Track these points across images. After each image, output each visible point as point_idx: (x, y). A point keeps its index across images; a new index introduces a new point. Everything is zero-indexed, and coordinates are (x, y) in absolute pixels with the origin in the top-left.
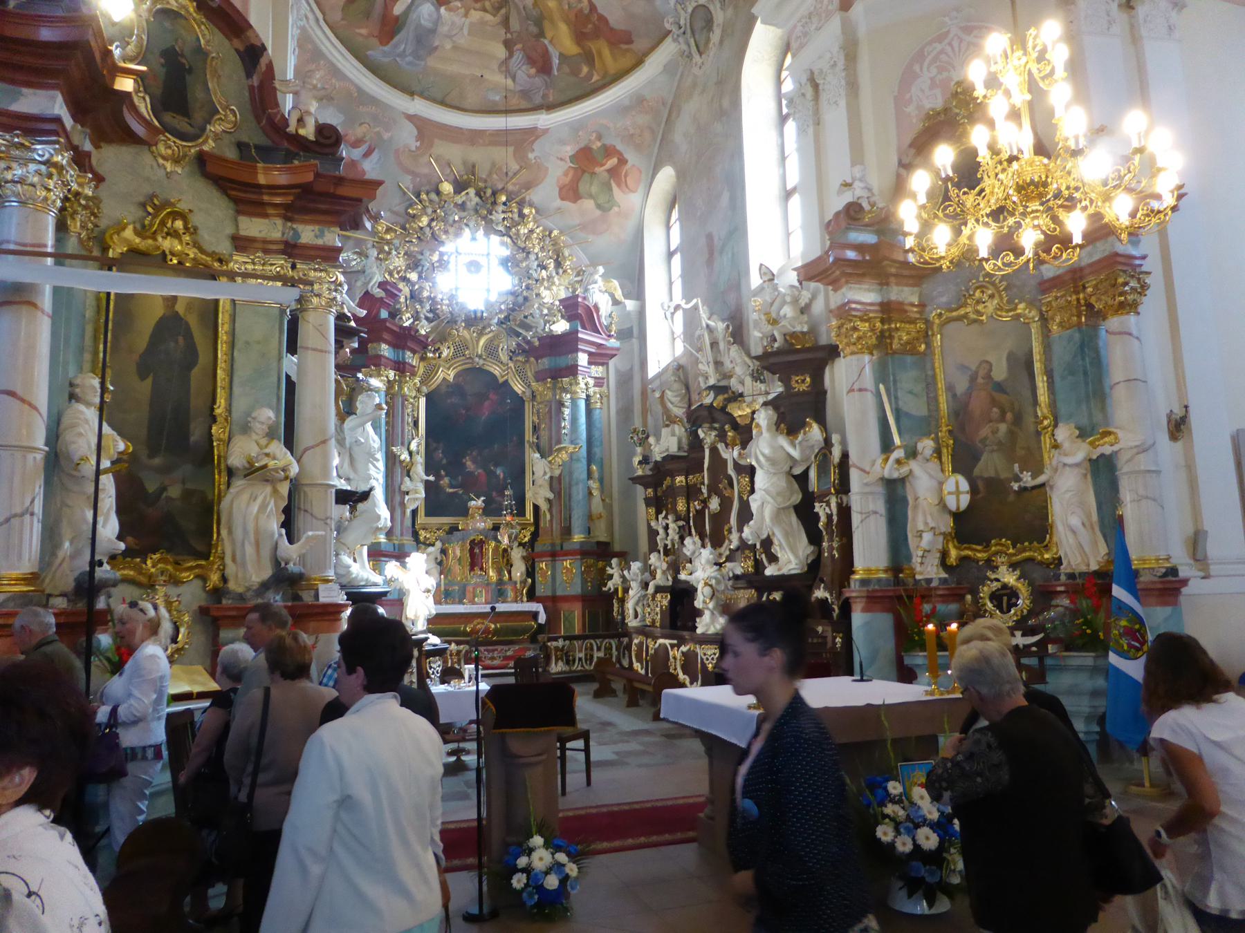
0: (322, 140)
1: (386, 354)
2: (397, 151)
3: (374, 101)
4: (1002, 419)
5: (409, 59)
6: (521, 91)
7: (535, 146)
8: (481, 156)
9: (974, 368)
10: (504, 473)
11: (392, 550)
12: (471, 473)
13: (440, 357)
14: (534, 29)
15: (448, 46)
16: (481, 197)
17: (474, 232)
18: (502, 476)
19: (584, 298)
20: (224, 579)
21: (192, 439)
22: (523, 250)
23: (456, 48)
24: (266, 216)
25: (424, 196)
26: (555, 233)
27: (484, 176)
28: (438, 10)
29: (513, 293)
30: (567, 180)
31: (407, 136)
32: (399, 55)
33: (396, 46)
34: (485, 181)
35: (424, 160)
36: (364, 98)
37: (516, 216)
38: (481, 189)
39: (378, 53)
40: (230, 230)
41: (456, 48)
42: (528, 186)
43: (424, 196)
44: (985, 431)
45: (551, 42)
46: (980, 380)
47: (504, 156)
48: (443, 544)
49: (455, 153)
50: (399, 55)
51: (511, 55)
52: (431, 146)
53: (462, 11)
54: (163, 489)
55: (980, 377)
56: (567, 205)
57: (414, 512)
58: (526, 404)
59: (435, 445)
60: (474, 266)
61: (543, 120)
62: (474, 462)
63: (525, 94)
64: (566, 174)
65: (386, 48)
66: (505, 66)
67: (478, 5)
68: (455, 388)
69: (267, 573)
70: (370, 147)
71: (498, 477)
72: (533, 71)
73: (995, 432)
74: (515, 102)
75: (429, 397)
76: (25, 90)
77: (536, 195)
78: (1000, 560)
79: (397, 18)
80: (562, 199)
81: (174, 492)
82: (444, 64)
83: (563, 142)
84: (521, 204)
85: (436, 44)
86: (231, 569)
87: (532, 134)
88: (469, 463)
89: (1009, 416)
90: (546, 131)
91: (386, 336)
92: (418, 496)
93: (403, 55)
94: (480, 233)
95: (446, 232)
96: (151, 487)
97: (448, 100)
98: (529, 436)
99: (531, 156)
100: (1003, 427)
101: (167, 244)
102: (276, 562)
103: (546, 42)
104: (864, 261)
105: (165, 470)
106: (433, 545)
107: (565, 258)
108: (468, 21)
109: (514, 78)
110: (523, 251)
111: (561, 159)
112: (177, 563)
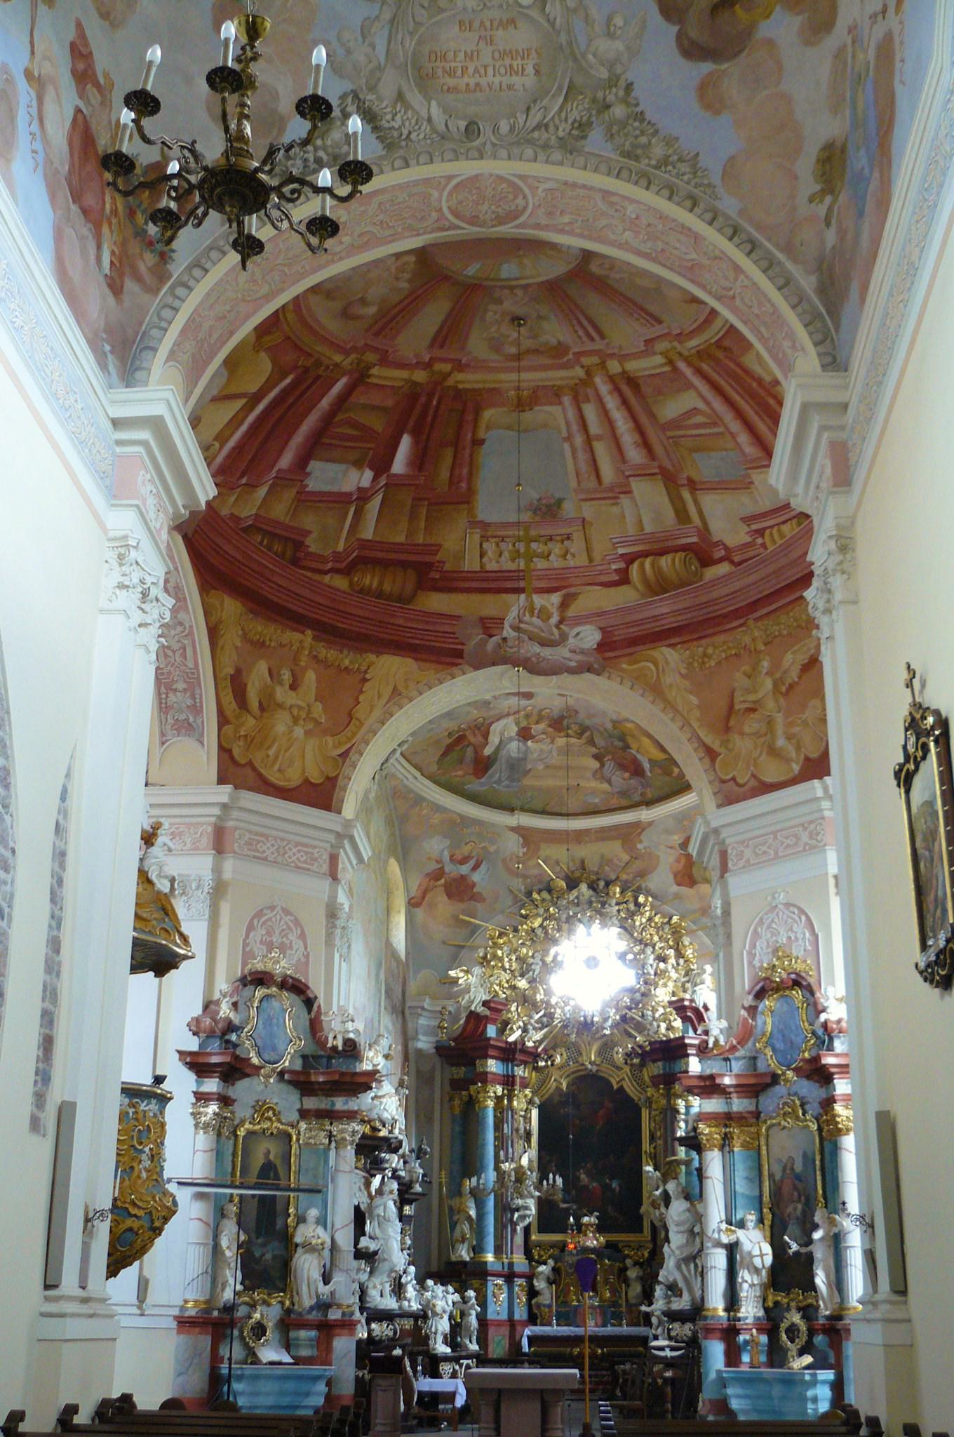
0: (347, 1048)
1: (494, 1069)
2: (504, 861)
3: (480, 823)
4: (799, 1201)
5: (507, 783)
6: (619, 793)
7: (643, 837)
8: (590, 853)
9: (784, 1161)
10: (621, 1187)
11: (501, 1269)
12: (586, 1187)
13: (552, 1065)
14: (620, 744)
15: (541, 767)
16: (594, 890)
17: (589, 927)
18: (617, 1189)
19: (692, 1001)
20: (293, 1304)
21: (278, 1227)
22: (641, 942)
23: (547, 767)
24: (317, 1095)
25: (535, 896)
26: (675, 919)
27: (596, 869)
28: (525, 744)
29: (632, 991)
30: (680, 866)
31: (512, 844)
32: (495, 783)
33: (491, 777)
34: (597, 873)
35: (532, 863)
36: (465, 821)
37: (632, 907)
38: (593, 882)
39: (475, 785)
40: (298, 1106)
41: (547, 767)
42: (642, 874)
43: (535, 896)
44: (790, 1209)
45: (638, 751)
46: (788, 1171)
47: (614, 849)
48: (556, 1263)
49: (559, 852)
50: (495, 783)
51: (602, 765)
52: (538, 849)
53: (549, 740)
54: (263, 1255)
55: (788, 1167)
56: (684, 890)
57: (527, 1230)
58: (643, 1110)
59: (548, 1158)
60: (592, 962)
61: (644, 815)
62: (589, 1175)
63: (623, 794)
64: (678, 861)
65: (483, 780)
66: (598, 775)
67: (562, 734)
68: (569, 1098)
69: (314, 1301)
70: (477, 860)
71: (614, 1190)
72: (627, 775)
73: (795, 1209)
74: (615, 802)
75: (540, 1108)
76: (206, 1080)
77: (653, 882)
78: (793, 1304)
79: (489, 757)
80: (679, 885)
81: (268, 1256)
82: (542, 781)
83: (667, 832)
84: (638, 891)
85: (529, 767)
86: (296, 1299)
87: (637, 828)
88: (583, 1176)
89: (803, 1198)
90: (650, 824)
91: (491, 1052)
92: (528, 1212)
93: (499, 781)
94: (596, 925)
95: (559, 930)
96: (257, 1254)
97: (548, 809)
98: (646, 1146)
99: (639, 846)
100: (800, 1206)
101: (266, 1125)
102: (318, 1296)
103: (634, 752)
104: (706, 1086)
105: (264, 1245)
106: (545, 1263)
107: (685, 946)
108: (554, 747)
109: (609, 782)
110: (641, 944)
111: (671, 848)
112: (269, 1294)
